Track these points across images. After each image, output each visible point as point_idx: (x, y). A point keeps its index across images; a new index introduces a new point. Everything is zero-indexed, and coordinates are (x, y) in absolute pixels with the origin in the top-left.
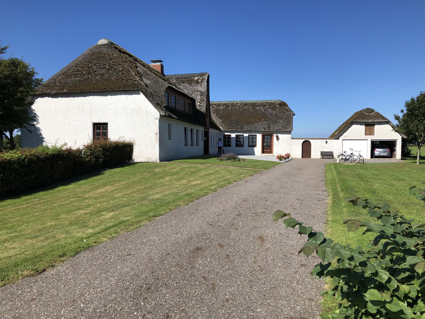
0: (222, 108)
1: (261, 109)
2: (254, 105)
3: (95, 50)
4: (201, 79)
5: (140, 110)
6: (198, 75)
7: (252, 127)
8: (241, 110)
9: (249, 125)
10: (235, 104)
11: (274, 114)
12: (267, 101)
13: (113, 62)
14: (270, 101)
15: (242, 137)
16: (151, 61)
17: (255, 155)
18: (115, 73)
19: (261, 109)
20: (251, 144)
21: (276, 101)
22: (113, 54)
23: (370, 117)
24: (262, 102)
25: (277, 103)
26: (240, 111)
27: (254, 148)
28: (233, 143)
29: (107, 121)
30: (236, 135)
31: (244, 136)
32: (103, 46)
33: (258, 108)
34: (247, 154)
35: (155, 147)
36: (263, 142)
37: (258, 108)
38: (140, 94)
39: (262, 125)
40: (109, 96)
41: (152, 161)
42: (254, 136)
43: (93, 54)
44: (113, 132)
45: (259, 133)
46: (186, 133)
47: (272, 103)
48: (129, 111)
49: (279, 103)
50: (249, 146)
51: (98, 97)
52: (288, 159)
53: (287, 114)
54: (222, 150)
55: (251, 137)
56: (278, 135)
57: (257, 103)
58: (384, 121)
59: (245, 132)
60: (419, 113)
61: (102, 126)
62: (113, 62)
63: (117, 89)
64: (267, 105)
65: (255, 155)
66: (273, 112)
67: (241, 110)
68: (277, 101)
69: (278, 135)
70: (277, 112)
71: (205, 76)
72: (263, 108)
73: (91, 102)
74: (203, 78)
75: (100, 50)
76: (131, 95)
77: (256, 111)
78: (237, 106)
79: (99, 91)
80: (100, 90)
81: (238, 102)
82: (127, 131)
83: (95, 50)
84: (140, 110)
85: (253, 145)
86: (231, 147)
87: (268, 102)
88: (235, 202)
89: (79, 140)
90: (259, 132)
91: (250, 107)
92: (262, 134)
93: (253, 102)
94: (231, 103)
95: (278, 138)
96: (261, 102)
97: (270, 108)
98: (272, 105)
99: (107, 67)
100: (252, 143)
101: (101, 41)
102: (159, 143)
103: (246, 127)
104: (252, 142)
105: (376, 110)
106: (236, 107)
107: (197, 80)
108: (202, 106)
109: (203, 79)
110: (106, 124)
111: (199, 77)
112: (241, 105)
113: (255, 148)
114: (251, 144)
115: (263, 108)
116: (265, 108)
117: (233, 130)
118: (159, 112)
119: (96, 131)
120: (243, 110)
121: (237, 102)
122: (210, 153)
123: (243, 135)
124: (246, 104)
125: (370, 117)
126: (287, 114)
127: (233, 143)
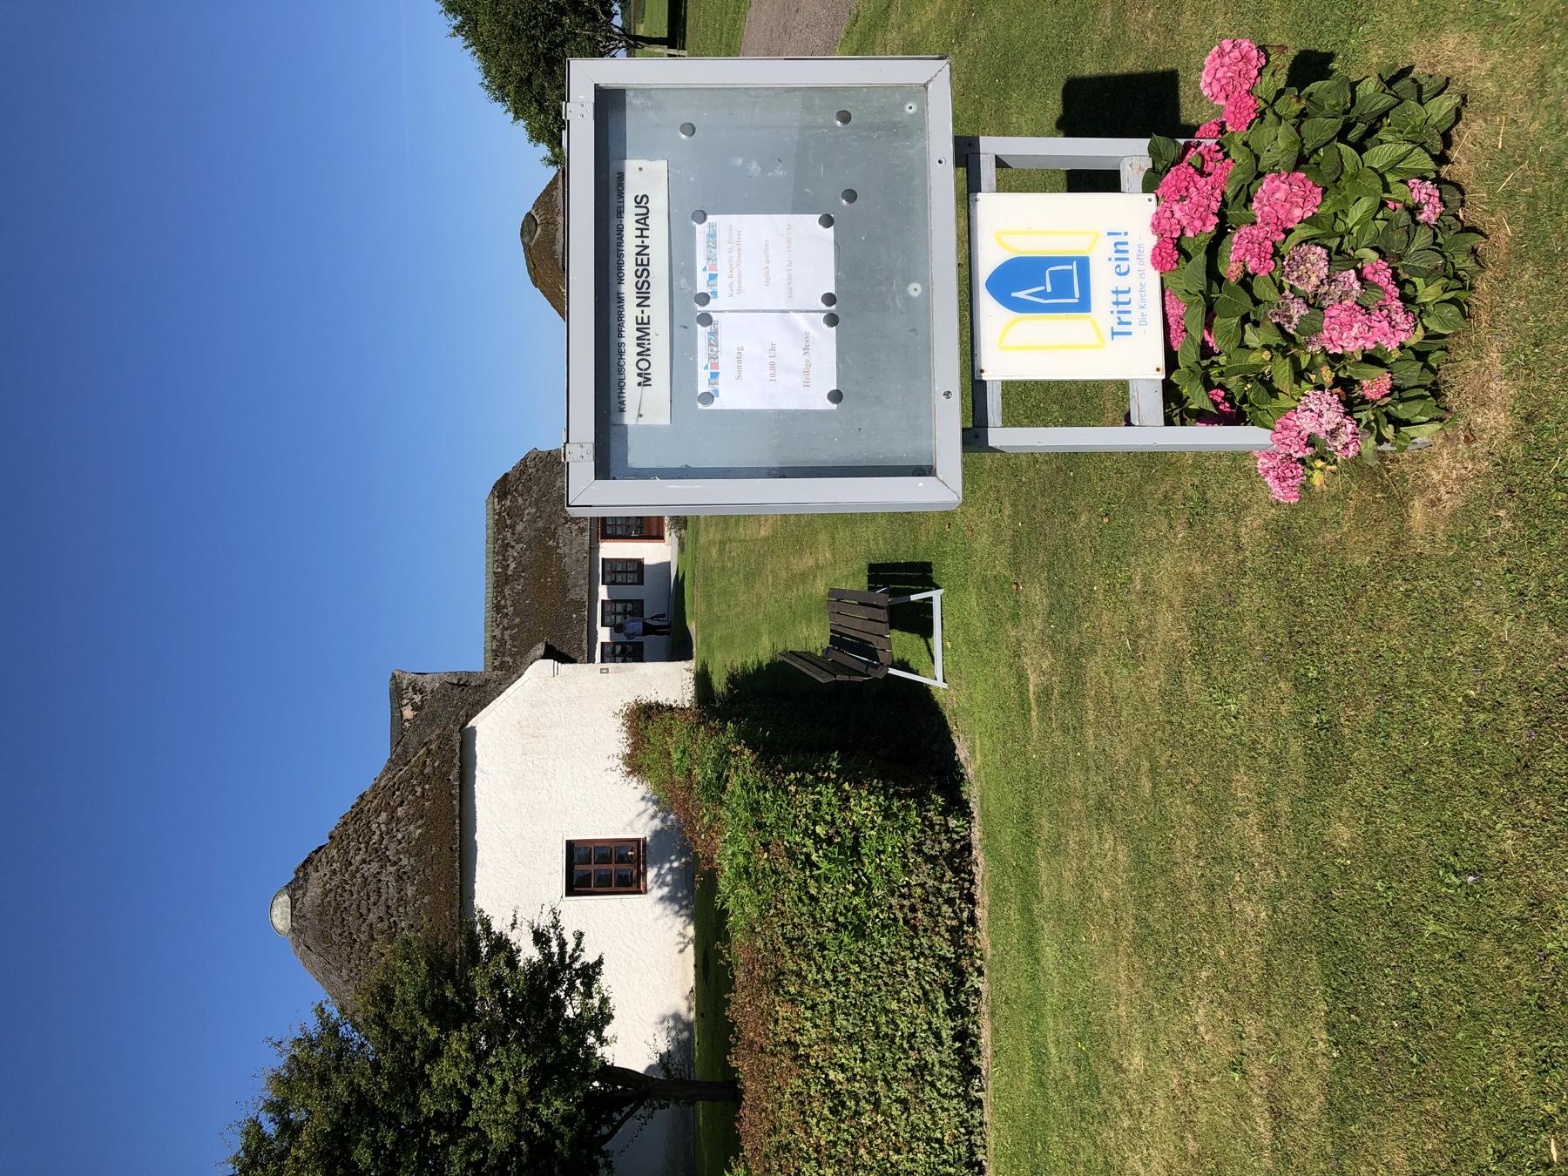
1: (515, 554)
2: (501, 581)
3: (309, 932)
4: (411, 694)
5: (528, 726)
6: (397, 708)
7: (578, 573)
8: (518, 620)
9: (570, 582)
10: (495, 643)
11: (534, 510)
12: (491, 540)
13: (360, 849)
14: (490, 531)
15: (608, 608)
17: (669, 563)
18: (398, 830)
19: (515, 554)
20: (632, 578)
21: (491, 512)
22: (328, 862)
23: (548, 223)
24: (491, 555)
25: (497, 507)
26: (522, 622)
27: (648, 566)
29: (559, 841)
31: (606, 598)
32: (298, 905)
33: (513, 566)
35: (646, 674)
36: (626, 537)
37: (513, 566)
38: (473, 728)
39: (570, 547)
40: (477, 837)
41: (690, 685)
42: (607, 569)
43: (324, 937)
44: (598, 821)
45: (598, 548)
47: (497, 524)
48: (530, 764)
49: (496, 500)
50: (640, 582)
51: (477, 879)
53: (534, 470)
54: (655, 623)
55: (608, 620)
57: (495, 573)
58: (560, 183)
59: (593, 594)
60: (545, 39)
61: (576, 867)
62: (360, 849)
63: (454, 802)
64: (505, 538)
65: (669, 563)
66: (528, 514)
67: (518, 620)
68: (490, 506)
70: (527, 503)
71: (401, 682)
72: (513, 547)
73: (495, 902)
74: (407, 688)
75: (312, 912)
76: (478, 761)
77: (517, 575)
78: (503, 635)
79: (460, 867)
80: (457, 864)
81: (489, 634)
82: (595, 772)
83: (309, 932)
84: (528, 726)
85: (666, 35)
87: (492, 535)
89: (624, 947)
90: (594, 549)
91: (507, 591)
93: (490, 585)
94: (490, 659)
96: (490, 560)
97: (513, 527)
98: (502, 524)
99: (375, 866)
100: (630, 572)
101: (276, 920)
102: (634, 664)
103: (579, 593)
104: (627, 572)
105: (529, 208)
106: (507, 637)
107: (415, 708)
109: (414, 688)
110: (570, 845)
111: (405, 701)
112: (498, 625)
113: (646, 562)
114: (632, 578)
115: (513, 547)
116: (513, 543)
117: (585, 632)
118: (535, 660)
119: (593, 888)
120: (516, 614)
121: (489, 639)
123: (603, 601)
124: (498, 608)
125: (548, 223)
126: (534, 470)
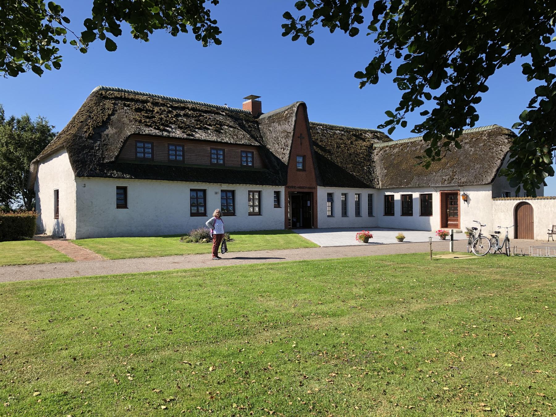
0: (396, 150)
16: (245, 98)
28: (398, 208)
30: (402, 195)
34: (411, 228)
46: (58, 205)
52: (402, 242)
56: (468, 193)
69: (468, 193)
86: (394, 215)
88: (255, 298)
90: (436, 189)
92: (441, 193)
95: (466, 199)
108: (285, 154)
117: (394, 187)
122: (318, 227)
127: (398, 208)
